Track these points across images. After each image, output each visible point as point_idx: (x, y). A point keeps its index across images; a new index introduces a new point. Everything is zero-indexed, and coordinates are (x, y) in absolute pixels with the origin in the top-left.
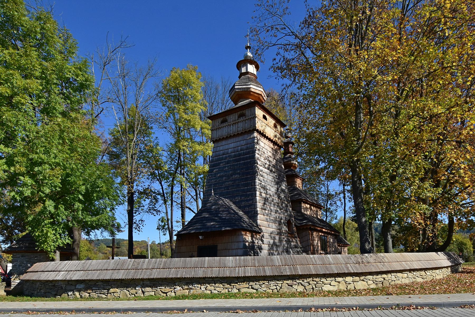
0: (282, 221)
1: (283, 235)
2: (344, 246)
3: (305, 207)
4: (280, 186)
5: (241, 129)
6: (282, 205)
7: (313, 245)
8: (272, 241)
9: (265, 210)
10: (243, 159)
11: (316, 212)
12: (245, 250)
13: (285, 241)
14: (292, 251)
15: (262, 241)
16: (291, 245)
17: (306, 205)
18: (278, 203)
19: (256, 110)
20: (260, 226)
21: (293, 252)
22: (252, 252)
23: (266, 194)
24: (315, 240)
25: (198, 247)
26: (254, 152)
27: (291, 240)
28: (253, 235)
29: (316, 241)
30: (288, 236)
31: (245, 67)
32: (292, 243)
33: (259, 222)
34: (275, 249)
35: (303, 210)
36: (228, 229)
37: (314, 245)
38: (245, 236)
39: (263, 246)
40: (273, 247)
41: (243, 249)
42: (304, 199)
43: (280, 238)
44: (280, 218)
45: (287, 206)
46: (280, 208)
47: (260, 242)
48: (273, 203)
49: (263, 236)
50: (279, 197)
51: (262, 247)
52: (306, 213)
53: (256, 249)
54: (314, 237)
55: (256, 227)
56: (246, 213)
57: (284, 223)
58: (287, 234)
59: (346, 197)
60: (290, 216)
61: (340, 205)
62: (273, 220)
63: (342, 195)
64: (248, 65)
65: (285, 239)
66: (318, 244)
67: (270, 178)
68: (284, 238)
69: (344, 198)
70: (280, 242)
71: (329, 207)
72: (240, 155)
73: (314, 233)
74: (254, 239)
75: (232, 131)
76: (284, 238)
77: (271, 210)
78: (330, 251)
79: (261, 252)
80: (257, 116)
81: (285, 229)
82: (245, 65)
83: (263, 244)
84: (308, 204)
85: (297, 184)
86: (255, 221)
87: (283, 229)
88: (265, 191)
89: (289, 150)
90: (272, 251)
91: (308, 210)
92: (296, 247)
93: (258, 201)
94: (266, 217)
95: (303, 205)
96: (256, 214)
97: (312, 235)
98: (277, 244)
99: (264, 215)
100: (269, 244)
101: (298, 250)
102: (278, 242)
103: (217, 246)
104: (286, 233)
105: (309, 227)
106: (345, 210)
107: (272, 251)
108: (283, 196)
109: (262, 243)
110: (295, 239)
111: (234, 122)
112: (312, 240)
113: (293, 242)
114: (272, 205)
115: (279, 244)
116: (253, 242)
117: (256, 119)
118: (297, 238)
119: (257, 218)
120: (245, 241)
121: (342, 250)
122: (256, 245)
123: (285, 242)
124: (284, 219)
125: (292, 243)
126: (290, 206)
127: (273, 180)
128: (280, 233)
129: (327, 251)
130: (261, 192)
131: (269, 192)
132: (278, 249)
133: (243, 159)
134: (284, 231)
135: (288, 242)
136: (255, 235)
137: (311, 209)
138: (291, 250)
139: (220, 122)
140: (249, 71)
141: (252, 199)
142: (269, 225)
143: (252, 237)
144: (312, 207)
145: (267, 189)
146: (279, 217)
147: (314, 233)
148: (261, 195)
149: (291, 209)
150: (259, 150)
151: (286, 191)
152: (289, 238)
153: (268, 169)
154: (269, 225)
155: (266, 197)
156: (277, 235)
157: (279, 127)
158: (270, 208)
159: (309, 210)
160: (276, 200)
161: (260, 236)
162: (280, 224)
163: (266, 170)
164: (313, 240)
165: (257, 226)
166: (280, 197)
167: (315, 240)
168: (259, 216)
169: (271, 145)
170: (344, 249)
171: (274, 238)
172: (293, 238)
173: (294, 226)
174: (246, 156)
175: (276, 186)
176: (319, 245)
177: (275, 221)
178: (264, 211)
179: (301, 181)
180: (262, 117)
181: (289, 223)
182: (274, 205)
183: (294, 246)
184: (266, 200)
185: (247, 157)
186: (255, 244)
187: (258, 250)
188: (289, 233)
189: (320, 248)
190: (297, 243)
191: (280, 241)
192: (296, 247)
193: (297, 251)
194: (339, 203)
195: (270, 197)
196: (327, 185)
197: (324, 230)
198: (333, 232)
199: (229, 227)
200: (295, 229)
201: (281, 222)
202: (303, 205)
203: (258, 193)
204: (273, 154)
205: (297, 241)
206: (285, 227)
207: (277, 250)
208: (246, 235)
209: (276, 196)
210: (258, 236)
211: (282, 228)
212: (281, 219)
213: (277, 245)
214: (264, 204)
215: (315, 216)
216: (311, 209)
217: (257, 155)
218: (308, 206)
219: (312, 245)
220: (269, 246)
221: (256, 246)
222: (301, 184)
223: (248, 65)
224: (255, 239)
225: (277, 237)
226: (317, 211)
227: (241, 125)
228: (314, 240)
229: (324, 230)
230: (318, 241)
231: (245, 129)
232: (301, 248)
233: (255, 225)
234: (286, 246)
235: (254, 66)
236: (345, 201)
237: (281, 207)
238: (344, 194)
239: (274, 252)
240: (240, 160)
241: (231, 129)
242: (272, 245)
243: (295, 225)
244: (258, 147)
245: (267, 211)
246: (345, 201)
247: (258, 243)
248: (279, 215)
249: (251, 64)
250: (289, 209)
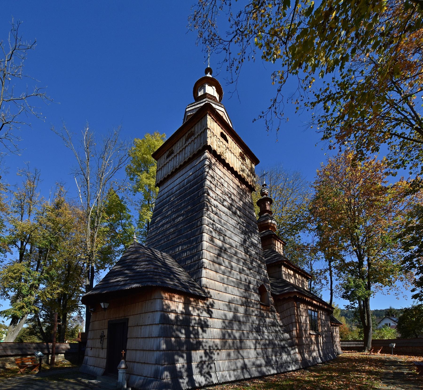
0: (251, 286)
1: (251, 306)
2: (336, 326)
3: (287, 272)
4: (249, 237)
5: (189, 154)
6: (252, 263)
7: (300, 323)
8: (230, 315)
9: (220, 264)
10: (189, 194)
11: (302, 281)
12: (163, 326)
13: (256, 315)
14: (266, 331)
15: (210, 313)
16: (265, 321)
17: (289, 271)
18: (245, 260)
19: (208, 119)
20: (207, 288)
21: (269, 333)
22: (183, 331)
23: (224, 241)
24: (302, 316)
25: (109, 322)
26: (204, 179)
27: (265, 314)
28: (191, 301)
29: (304, 317)
30: (260, 309)
31: (203, 90)
32: (267, 320)
33: (204, 281)
34: (235, 327)
35: (284, 276)
36: (134, 286)
37: (301, 322)
38: (167, 302)
39: (210, 321)
40: (233, 324)
41: (160, 325)
42: (285, 261)
43: (246, 311)
44: (248, 281)
45: (259, 266)
46: (249, 267)
47: (205, 314)
48: (236, 257)
49: (212, 305)
50: (247, 252)
51: (209, 323)
52: (288, 280)
53: (193, 327)
54: (300, 311)
55: (198, 288)
56: (180, 262)
57: (253, 289)
58: (259, 306)
59: (333, 274)
60: (265, 281)
61: (325, 283)
62: (233, 282)
63: (327, 274)
64: (207, 86)
65: (256, 312)
66: (306, 321)
67: (233, 222)
68: (253, 311)
69: (331, 275)
70: (247, 317)
71: (313, 286)
72: (186, 189)
73: (301, 306)
74: (191, 308)
75: (178, 162)
76: (254, 311)
77: (232, 267)
78: (322, 331)
79: (204, 331)
80: (208, 127)
81: (255, 297)
82: (203, 87)
83: (211, 317)
84: (291, 269)
85: (277, 247)
86: (199, 279)
87: (252, 298)
88: (222, 238)
89: (266, 207)
90: (229, 331)
91: (291, 278)
92: (274, 324)
93: (205, 247)
94: (222, 276)
95: (284, 269)
96: (201, 266)
97: (298, 307)
98: (241, 319)
99: (217, 272)
100: (224, 317)
101: (277, 329)
102: (243, 317)
103: (128, 319)
104: (257, 305)
105: (292, 296)
106: (331, 290)
107: (229, 331)
108: (253, 253)
109: (207, 315)
110: (272, 314)
111: (181, 149)
112: (298, 315)
113: (269, 317)
114: (234, 260)
115: (244, 319)
116: (187, 314)
117: (209, 132)
118: (274, 312)
119: (201, 275)
120: (166, 310)
121: (333, 330)
122: (195, 319)
123: (255, 317)
124: (255, 283)
125: (267, 320)
126: (265, 267)
127: (238, 227)
128: (246, 303)
129: (318, 330)
130: (212, 236)
131: (228, 240)
132: (243, 327)
133: (189, 194)
134: (253, 301)
135: (261, 317)
136: (194, 301)
137: (295, 277)
138: (264, 329)
139: (166, 158)
140: (206, 92)
141: (197, 246)
142: (226, 289)
143: (187, 304)
144: (297, 275)
145: (226, 236)
146: (246, 280)
147: (301, 306)
148: (212, 240)
149: (266, 271)
150: (213, 177)
151: (260, 246)
152: (263, 312)
153: (229, 209)
154: (226, 289)
155: (223, 245)
156: (241, 305)
157: (248, 161)
158: (229, 263)
159: (293, 278)
160: (242, 254)
161: (205, 304)
162: (247, 289)
163: (226, 210)
164: (300, 315)
165: (201, 287)
166: (248, 251)
167: (302, 316)
168: (204, 271)
169: (237, 181)
170: (335, 329)
171: (236, 311)
172: (269, 311)
173: (270, 295)
174: (192, 188)
175: (243, 236)
176: (308, 322)
177: (238, 284)
178: (217, 266)
179: (281, 245)
180: (219, 134)
181: (261, 290)
182: (238, 260)
183: (270, 323)
184: (222, 251)
185: (194, 189)
186: (193, 317)
187: (199, 328)
188: (261, 304)
189: (308, 327)
190: (275, 318)
191: (247, 314)
192: (274, 324)
193: (276, 331)
194: (324, 282)
195: (230, 248)
196: (311, 263)
197: (314, 302)
198: (326, 307)
199: (137, 283)
200: (271, 299)
201: (249, 287)
202: (284, 269)
203: (206, 237)
204: (239, 194)
205: (274, 316)
206: (256, 295)
207: (240, 329)
208: (171, 300)
209: (242, 249)
210: (201, 304)
211: (250, 296)
212: (250, 283)
213: (239, 321)
214: (219, 255)
215: (300, 286)
216: (295, 277)
217: (208, 183)
218: (292, 272)
219: (298, 322)
220: (224, 322)
221: (193, 322)
222: (282, 248)
223: (207, 86)
224: (193, 308)
225: (242, 309)
226: (303, 281)
227: (188, 149)
228: (300, 315)
229: (314, 302)
230: (306, 317)
231: (193, 152)
232: (281, 326)
233: (198, 286)
234: (257, 323)
235: (214, 87)
236: (331, 278)
237: (250, 266)
238: (331, 271)
239: (234, 331)
240: (185, 196)
241: (178, 159)
242: (231, 322)
243: (272, 295)
244: (210, 172)
245: (223, 268)
246: (331, 278)
247: (199, 315)
248: (246, 276)
249: (210, 85)
250: (264, 272)
